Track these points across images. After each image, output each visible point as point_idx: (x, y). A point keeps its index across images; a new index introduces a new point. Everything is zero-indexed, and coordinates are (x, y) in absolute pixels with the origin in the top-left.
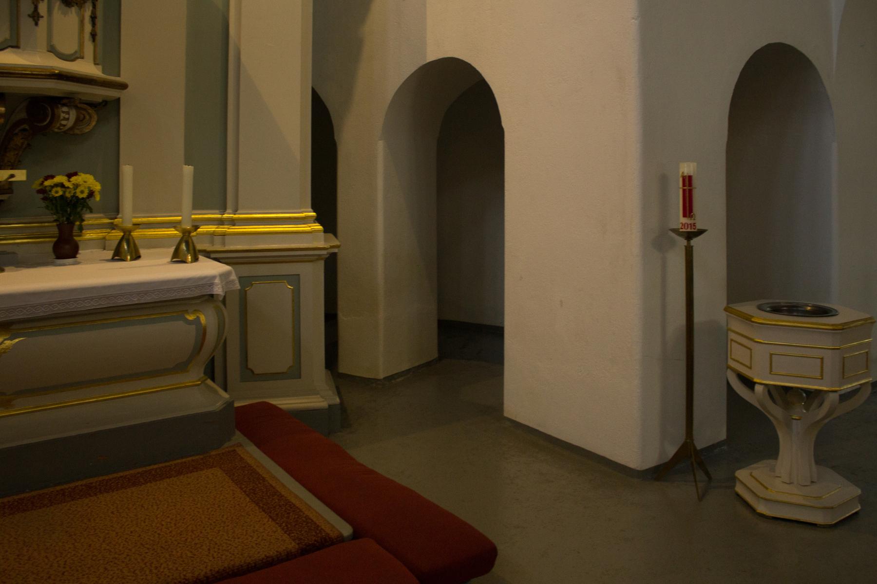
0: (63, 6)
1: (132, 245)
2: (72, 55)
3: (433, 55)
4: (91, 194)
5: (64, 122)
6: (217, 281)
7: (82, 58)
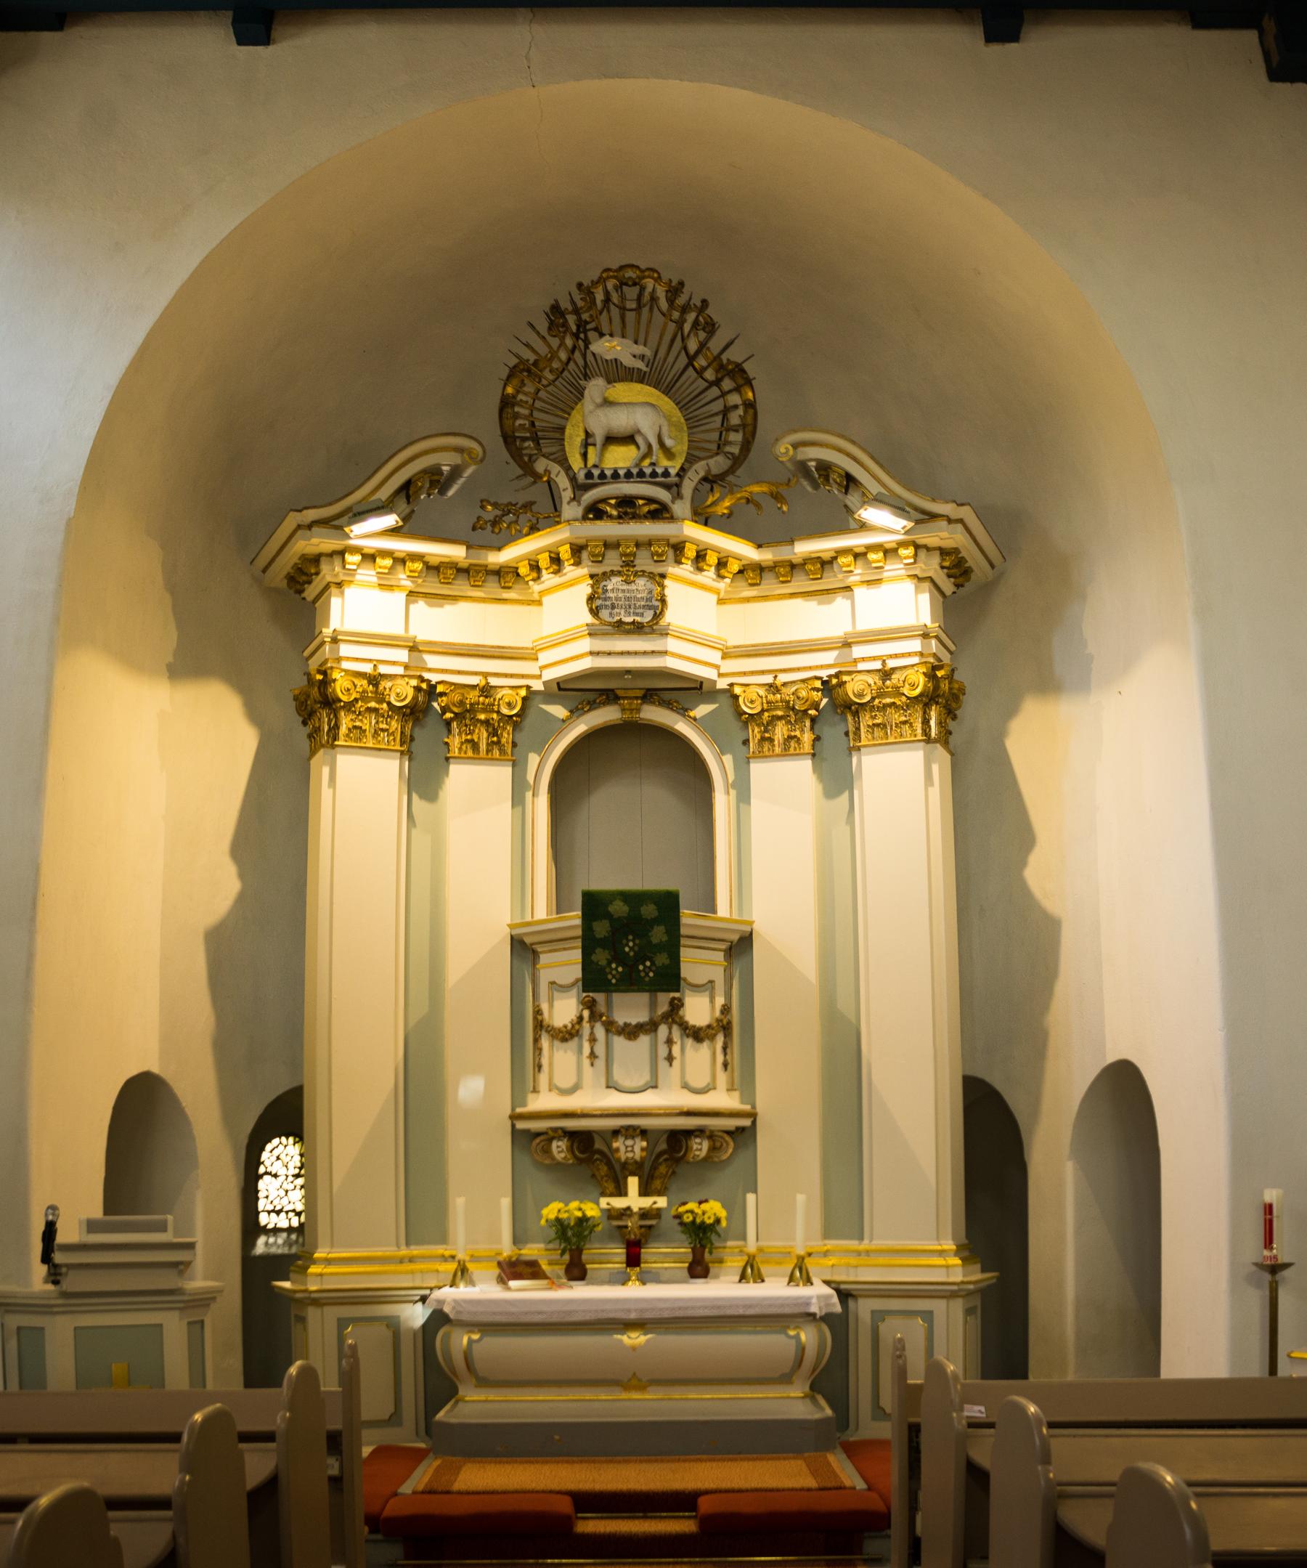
0: (695, 1043)
2: (704, 1088)
3: (1110, 1059)
5: (697, 1153)
6: (814, 1301)
7: (715, 1088)
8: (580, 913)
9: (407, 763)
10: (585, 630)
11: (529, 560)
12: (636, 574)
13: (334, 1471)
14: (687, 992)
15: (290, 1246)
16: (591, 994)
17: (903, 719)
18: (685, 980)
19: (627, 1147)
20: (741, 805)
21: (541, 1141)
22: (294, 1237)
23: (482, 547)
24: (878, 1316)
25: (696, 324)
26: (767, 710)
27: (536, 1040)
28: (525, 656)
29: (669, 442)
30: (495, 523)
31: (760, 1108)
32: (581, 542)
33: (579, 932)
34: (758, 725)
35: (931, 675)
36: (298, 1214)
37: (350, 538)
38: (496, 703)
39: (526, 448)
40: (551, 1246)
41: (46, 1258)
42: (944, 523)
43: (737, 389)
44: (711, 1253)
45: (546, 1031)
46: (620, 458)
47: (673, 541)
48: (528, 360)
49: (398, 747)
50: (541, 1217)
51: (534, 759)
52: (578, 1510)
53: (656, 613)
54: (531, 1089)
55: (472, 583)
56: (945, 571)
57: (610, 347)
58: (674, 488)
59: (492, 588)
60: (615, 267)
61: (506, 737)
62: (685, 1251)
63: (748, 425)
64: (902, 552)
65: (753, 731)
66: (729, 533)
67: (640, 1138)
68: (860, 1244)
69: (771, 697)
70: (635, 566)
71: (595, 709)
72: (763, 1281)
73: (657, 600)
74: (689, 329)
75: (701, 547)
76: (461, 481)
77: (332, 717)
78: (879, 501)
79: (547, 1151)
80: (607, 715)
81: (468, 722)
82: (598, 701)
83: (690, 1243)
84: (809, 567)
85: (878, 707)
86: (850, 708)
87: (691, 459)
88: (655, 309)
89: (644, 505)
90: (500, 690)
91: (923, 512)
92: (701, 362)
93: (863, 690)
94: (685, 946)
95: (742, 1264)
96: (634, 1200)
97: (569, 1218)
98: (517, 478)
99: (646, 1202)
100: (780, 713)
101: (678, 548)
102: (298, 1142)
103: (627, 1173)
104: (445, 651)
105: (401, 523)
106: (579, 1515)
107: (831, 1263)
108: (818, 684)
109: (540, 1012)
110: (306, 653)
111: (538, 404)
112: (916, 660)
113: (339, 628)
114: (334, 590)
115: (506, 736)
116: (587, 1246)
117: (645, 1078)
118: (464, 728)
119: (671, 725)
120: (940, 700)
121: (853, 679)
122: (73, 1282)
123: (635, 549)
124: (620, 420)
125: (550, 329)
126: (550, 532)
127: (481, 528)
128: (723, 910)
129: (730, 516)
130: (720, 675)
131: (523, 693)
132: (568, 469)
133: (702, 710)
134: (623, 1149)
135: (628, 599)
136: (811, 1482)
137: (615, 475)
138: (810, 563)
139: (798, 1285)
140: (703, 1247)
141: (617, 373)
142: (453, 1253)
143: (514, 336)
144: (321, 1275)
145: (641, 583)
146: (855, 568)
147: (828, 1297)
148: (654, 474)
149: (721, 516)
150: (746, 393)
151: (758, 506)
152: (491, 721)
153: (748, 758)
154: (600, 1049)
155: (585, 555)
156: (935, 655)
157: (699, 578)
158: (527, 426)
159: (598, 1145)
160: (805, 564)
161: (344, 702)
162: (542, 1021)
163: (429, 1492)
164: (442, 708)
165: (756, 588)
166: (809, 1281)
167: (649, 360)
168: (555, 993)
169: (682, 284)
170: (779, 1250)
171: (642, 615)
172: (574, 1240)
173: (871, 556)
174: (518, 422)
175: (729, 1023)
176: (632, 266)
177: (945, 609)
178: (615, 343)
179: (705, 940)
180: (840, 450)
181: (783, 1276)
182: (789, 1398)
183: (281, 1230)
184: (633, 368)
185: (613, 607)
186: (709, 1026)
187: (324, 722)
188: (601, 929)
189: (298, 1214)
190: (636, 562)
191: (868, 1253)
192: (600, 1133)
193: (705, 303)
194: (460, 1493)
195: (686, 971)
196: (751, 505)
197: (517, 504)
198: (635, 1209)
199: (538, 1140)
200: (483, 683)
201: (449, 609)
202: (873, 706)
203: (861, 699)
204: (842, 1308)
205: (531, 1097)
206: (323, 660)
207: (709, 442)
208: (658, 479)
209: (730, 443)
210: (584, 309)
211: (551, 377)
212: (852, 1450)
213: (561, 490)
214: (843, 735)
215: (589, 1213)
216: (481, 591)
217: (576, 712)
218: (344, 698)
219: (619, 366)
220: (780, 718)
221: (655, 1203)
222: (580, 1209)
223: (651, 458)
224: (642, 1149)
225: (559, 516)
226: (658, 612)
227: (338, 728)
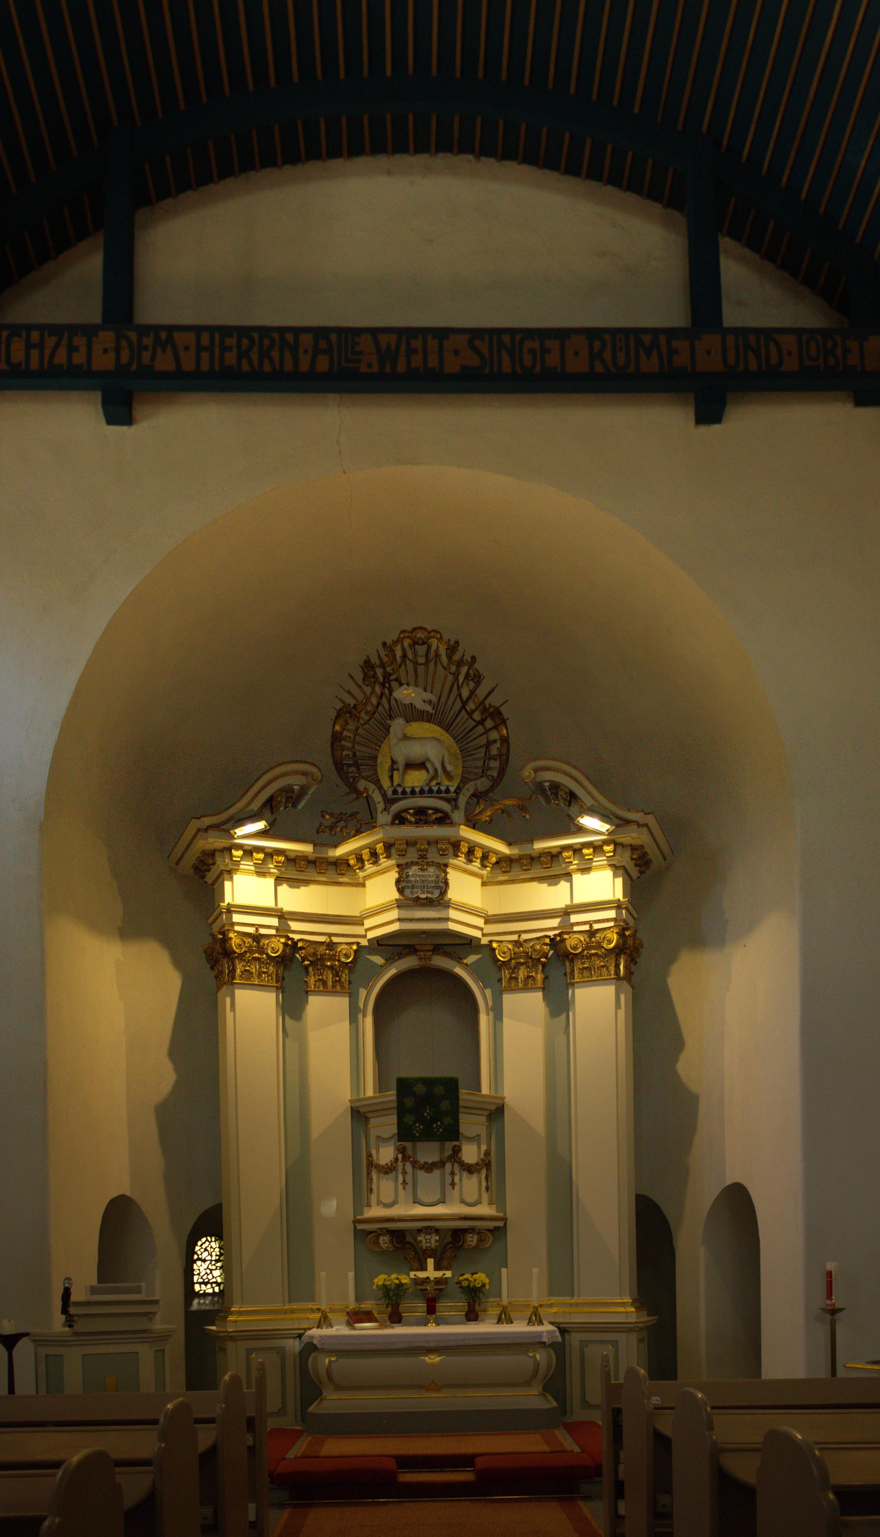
0: (468, 1175)
1: (507, 1315)
2: (473, 1203)
3: (728, 1183)
4: (484, 1285)
5: (471, 1243)
6: (545, 1334)
7: (481, 1203)
8: (395, 1092)
9: (281, 995)
10: (394, 904)
11: (356, 854)
12: (428, 864)
13: (250, 1443)
14: (463, 1142)
15: (214, 1304)
16: (403, 1143)
17: (603, 964)
18: (462, 1134)
20: (497, 1022)
21: (374, 1236)
22: (216, 1299)
23: (323, 845)
24: (584, 1344)
25: (467, 675)
26: (514, 959)
27: (369, 1173)
28: (354, 922)
29: (449, 768)
30: (332, 828)
31: (509, 1215)
32: (391, 841)
33: (395, 1105)
34: (508, 969)
35: (621, 935)
36: (218, 1284)
37: (235, 839)
39: (351, 772)
40: (380, 1302)
41: (65, 1311)
42: (635, 827)
43: (496, 727)
44: (479, 1305)
45: (375, 1168)
46: (416, 779)
47: (452, 840)
48: (350, 705)
49: (275, 984)
50: (373, 1283)
51: (363, 993)
52: (400, 1468)
53: (441, 892)
55: (318, 871)
56: (634, 861)
57: (407, 694)
58: (453, 802)
59: (332, 875)
60: (410, 628)
61: (345, 977)
62: (463, 1304)
63: (503, 755)
64: (606, 848)
65: (505, 973)
66: (489, 834)
67: (434, 1234)
68: (572, 1299)
69: (516, 950)
70: (427, 858)
71: (402, 958)
72: (512, 1323)
73: (442, 882)
74: (463, 678)
75: (471, 845)
76: (307, 797)
77: (230, 963)
78: (592, 811)
79: (376, 1243)
80: (409, 962)
81: (319, 967)
82: (404, 953)
83: (467, 1300)
84: (543, 859)
85: (586, 956)
86: (568, 957)
87: (464, 781)
88: (439, 665)
89: (433, 814)
90: (339, 945)
91: (621, 819)
92: (471, 706)
93: (577, 945)
94: (461, 1113)
95: (499, 1312)
97: (391, 1285)
98: (346, 794)
99: (439, 1274)
100: (522, 961)
101: (456, 846)
102: (218, 1240)
103: (426, 1256)
104: (302, 918)
105: (268, 828)
106: (400, 1470)
107: (554, 1311)
108: (547, 941)
110: (210, 921)
111: (358, 738)
112: (612, 924)
114: (226, 876)
115: (344, 976)
116: (401, 1303)
117: (438, 1196)
119: (451, 969)
120: (627, 951)
121: (570, 937)
122: (81, 1326)
123: (427, 846)
124: (415, 751)
125: (364, 679)
126: (369, 833)
127: (322, 831)
128: (485, 1090)
129: (491, 820)
130: (483, 935)
131: (355, 947)
132: (380, 788)
133: (471, 959)
134: (424, 1241)
136: (546, 1448)
137: (413, 792)
138: (543, 857)
139: (534, 1325)
140: (474, 1302)
141: (413, 714)
142: (319, 1307)
143: (339, 685)
144: (235, 1321)
145: (431, 870)
146: (574, 860)
147: (553, 1332)
148: (439, 791)
149: (485, 822)
150: (502, 730)
151: (509, 815)
152: (334, 967)
153: (501, 991)
154: (409, 1179)
155: (393, 851)
156: (624, 920)
157: (470, 867)
158: (351, 756)
159: (409, 1239)
160: (540, 857)
161: (238, 954)
162: (372, 1162)
163: (305, 1457)
164: (302, 958)
165: (507, 874)
166: (541, 1323)
168: (380, 1143)
169: (457, 643)
170: (521, 1303)
171: (432, 893)
172: (394, 1298)
173: (585, 851)
174: (345, 753)
175: (490, 1161)
176: (421, 628)
177: (632, 888)
178: (410, 691)
179: (473, 1110)
180: (567, 774)
181: (525, 1320)
182: (529, 1395)
183: (209, 1294)
184: (424, 711)
185: (413, 887)
186: (477, 1164)
187: (225, 967)
188: (409, 1102)
189: (218, 1284)
190: (428, 855)
191: (577, 1305)
192: (409, 1231)
193: (473, 658)
194: (325, 1457)
195: (463, 1129)
196: (505, 815)
197: (346, 814)
198: (432, 1279)
199: (370, 1236)
200: (328, 940)
201: (304, 890)
202: (583, 956)
203: (575, 951)
204: (562, 1338)
205: (366, 1209)
206: (221, 925)
207: (477, 768)
208: (442, 795)
209: (490, 769)
210: (388, 664)
211: (366, 718)
212: (570, 1428)
213: (376, 803)
214: (563, 975)
215: (404, 1281)
216: (324, 877)
218: (238, 951)
220: (522, 964)
221: (444, 1274)
222: (398, 1279)
223: (437, 779)
224: (436, 1241)
225: (375, 822)
226: (443, 891)
227: (235, 971)
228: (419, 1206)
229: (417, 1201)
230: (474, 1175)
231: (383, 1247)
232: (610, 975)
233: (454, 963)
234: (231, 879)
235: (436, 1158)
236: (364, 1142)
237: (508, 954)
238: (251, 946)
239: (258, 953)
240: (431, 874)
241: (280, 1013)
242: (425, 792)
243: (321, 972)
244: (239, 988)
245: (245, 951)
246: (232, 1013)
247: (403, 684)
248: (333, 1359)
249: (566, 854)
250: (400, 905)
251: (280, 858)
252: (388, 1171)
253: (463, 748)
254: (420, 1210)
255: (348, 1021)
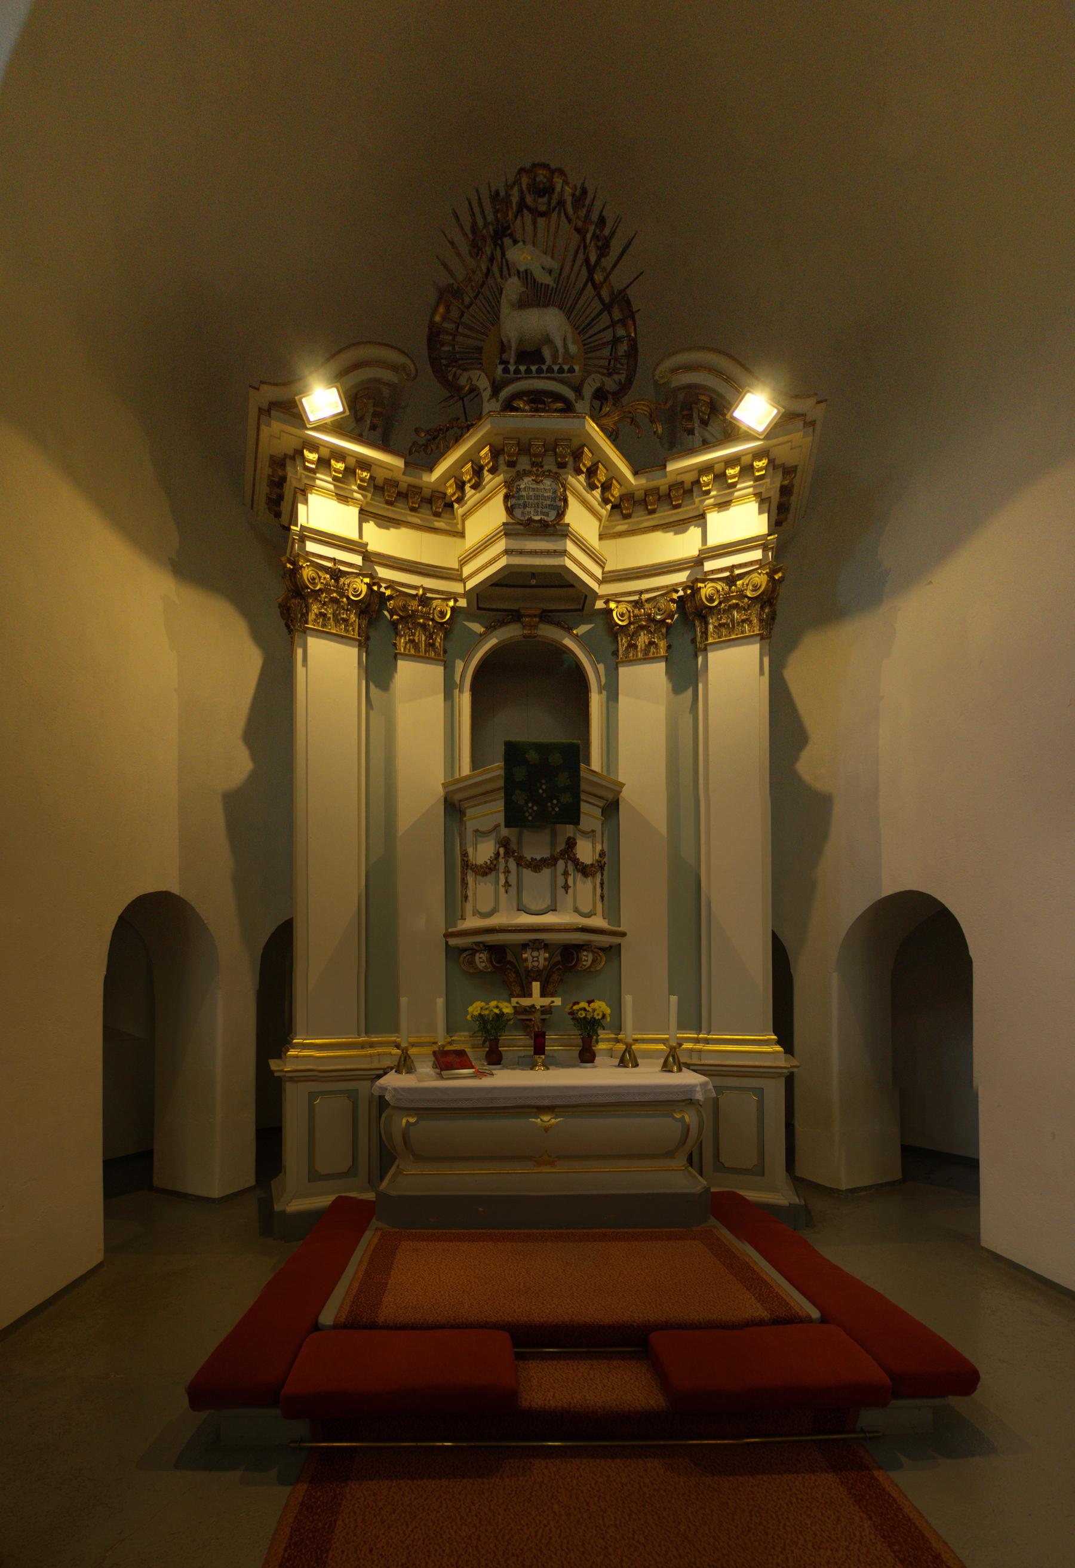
0: (583, 878)
3: (888, 889)
5: (584, 963)
6: (698, 1089)
7: (595, 915)
8: (502, 764)
12: (543, 474)
17: (745, 617)
19: (533, 957)
20: (610, 702)
21: (467, 956)
28: (452, 576)
33: (501, 783)
34: (626, 636)
38: (431, 612)
45: (471, 868)
51: (459, 665)
53: (558, 513)
54: (460, 917)
64: (758, 464)
69: (636, 611)
79: (472, 963)
96: (536, 999)
97: (489, 1014)
99: (546, 1001)
109: (466, 855)
113: (305, 524)
114: (300, 497)
117: (546, 903)
118: (407, 631)
119: (560, 640)
121: (705, 586)
133: (582, 629)
134: (530, 959)
135: (537, 497)
144: (297, 1057)
154: (513, 879)
159: (510, 957)
162: (467, 861)
167: (553, 288)
171: (547, 515)
172: (493, 1031)
184: (542, 284)
185: (525, 506)
188: (520, 774)
199: (464, 955)
202: (720, 610)
205: (459, 922)
208: (564, 375)
215: (506, 1011)
216: (417, 517)
217: (490, 628)
219: (529, 278)
221: (553, 1002)
222: (497, 1007)
224: (545, 959)
226: (560, 512)
228: (525, 914)
229: (521, 909)
230: (589, 879)
231: (479, 966)
232: (754, 631)
233: (563, 633)
234: (306, 502)
235: (546, 854)
236: (458, 842)
237: (626, 617)
238: (327, 584)
239: (336, 593)
240: (546, 488)
241: (363, 675)
242: (543, 370)
243: (412, 632)
244: (312, 636)
245: (320, 589)
246: (305, 668)
247: (518, 242)
248: (412, 1120)
249: (705, 479)
250: (508, 531)
251: (365, 474)
252: (487, 870)
253: (586, 342)
254: (525, 919)
255: (443, 695)
